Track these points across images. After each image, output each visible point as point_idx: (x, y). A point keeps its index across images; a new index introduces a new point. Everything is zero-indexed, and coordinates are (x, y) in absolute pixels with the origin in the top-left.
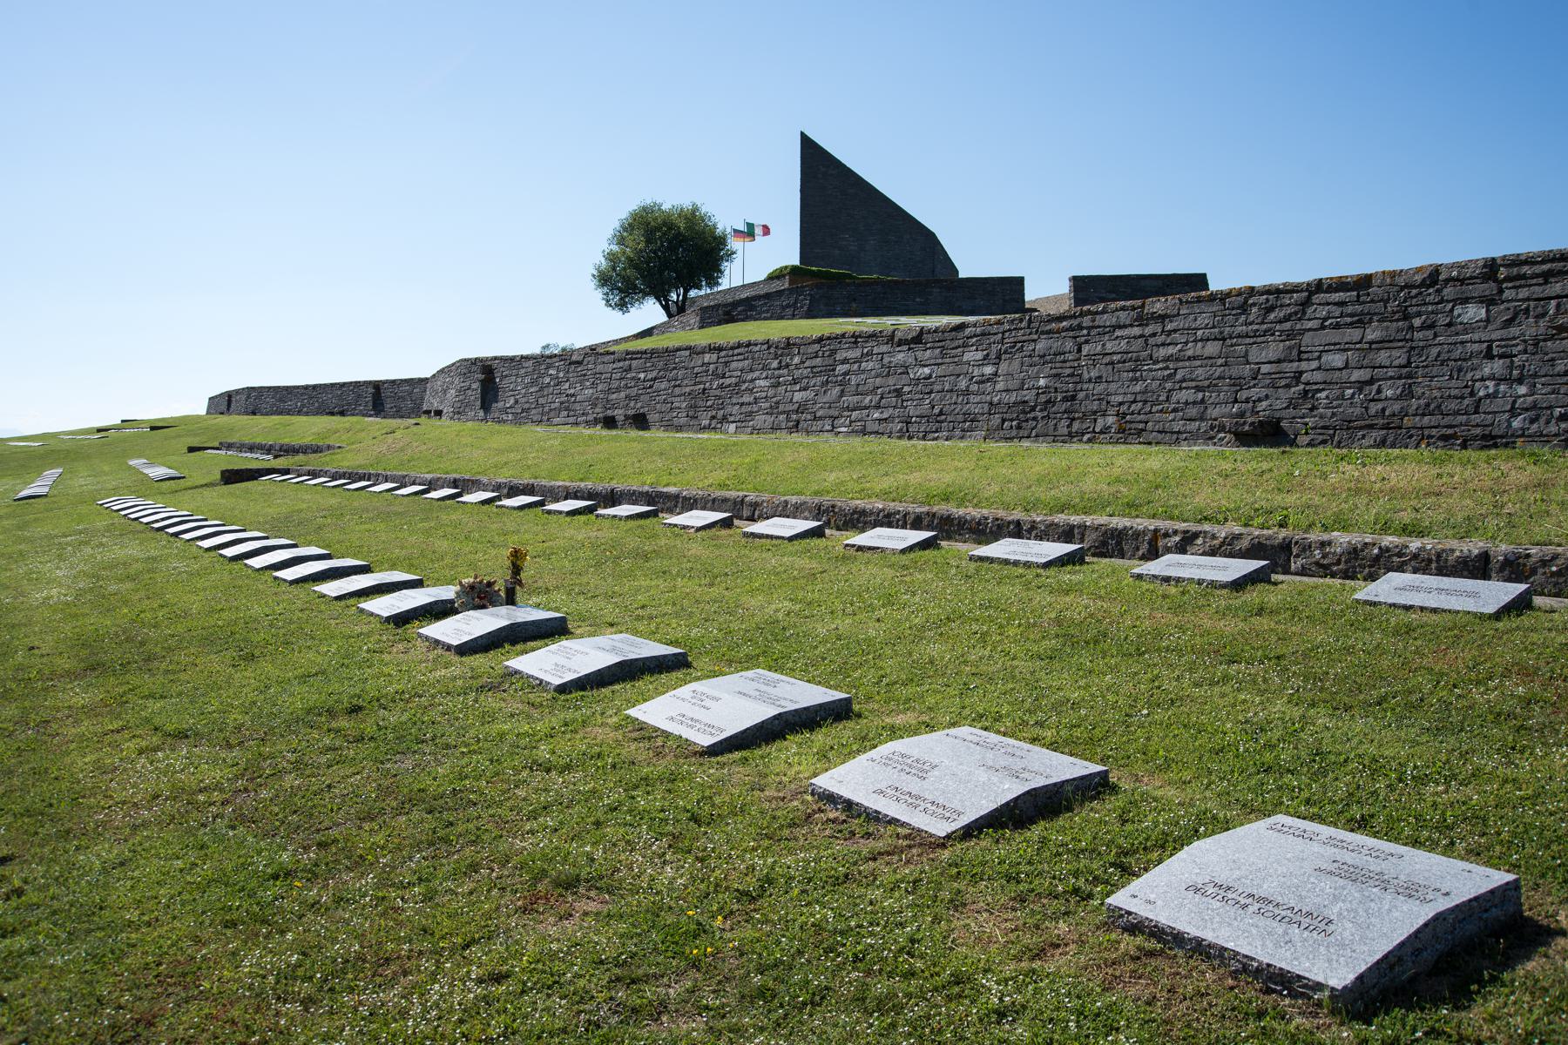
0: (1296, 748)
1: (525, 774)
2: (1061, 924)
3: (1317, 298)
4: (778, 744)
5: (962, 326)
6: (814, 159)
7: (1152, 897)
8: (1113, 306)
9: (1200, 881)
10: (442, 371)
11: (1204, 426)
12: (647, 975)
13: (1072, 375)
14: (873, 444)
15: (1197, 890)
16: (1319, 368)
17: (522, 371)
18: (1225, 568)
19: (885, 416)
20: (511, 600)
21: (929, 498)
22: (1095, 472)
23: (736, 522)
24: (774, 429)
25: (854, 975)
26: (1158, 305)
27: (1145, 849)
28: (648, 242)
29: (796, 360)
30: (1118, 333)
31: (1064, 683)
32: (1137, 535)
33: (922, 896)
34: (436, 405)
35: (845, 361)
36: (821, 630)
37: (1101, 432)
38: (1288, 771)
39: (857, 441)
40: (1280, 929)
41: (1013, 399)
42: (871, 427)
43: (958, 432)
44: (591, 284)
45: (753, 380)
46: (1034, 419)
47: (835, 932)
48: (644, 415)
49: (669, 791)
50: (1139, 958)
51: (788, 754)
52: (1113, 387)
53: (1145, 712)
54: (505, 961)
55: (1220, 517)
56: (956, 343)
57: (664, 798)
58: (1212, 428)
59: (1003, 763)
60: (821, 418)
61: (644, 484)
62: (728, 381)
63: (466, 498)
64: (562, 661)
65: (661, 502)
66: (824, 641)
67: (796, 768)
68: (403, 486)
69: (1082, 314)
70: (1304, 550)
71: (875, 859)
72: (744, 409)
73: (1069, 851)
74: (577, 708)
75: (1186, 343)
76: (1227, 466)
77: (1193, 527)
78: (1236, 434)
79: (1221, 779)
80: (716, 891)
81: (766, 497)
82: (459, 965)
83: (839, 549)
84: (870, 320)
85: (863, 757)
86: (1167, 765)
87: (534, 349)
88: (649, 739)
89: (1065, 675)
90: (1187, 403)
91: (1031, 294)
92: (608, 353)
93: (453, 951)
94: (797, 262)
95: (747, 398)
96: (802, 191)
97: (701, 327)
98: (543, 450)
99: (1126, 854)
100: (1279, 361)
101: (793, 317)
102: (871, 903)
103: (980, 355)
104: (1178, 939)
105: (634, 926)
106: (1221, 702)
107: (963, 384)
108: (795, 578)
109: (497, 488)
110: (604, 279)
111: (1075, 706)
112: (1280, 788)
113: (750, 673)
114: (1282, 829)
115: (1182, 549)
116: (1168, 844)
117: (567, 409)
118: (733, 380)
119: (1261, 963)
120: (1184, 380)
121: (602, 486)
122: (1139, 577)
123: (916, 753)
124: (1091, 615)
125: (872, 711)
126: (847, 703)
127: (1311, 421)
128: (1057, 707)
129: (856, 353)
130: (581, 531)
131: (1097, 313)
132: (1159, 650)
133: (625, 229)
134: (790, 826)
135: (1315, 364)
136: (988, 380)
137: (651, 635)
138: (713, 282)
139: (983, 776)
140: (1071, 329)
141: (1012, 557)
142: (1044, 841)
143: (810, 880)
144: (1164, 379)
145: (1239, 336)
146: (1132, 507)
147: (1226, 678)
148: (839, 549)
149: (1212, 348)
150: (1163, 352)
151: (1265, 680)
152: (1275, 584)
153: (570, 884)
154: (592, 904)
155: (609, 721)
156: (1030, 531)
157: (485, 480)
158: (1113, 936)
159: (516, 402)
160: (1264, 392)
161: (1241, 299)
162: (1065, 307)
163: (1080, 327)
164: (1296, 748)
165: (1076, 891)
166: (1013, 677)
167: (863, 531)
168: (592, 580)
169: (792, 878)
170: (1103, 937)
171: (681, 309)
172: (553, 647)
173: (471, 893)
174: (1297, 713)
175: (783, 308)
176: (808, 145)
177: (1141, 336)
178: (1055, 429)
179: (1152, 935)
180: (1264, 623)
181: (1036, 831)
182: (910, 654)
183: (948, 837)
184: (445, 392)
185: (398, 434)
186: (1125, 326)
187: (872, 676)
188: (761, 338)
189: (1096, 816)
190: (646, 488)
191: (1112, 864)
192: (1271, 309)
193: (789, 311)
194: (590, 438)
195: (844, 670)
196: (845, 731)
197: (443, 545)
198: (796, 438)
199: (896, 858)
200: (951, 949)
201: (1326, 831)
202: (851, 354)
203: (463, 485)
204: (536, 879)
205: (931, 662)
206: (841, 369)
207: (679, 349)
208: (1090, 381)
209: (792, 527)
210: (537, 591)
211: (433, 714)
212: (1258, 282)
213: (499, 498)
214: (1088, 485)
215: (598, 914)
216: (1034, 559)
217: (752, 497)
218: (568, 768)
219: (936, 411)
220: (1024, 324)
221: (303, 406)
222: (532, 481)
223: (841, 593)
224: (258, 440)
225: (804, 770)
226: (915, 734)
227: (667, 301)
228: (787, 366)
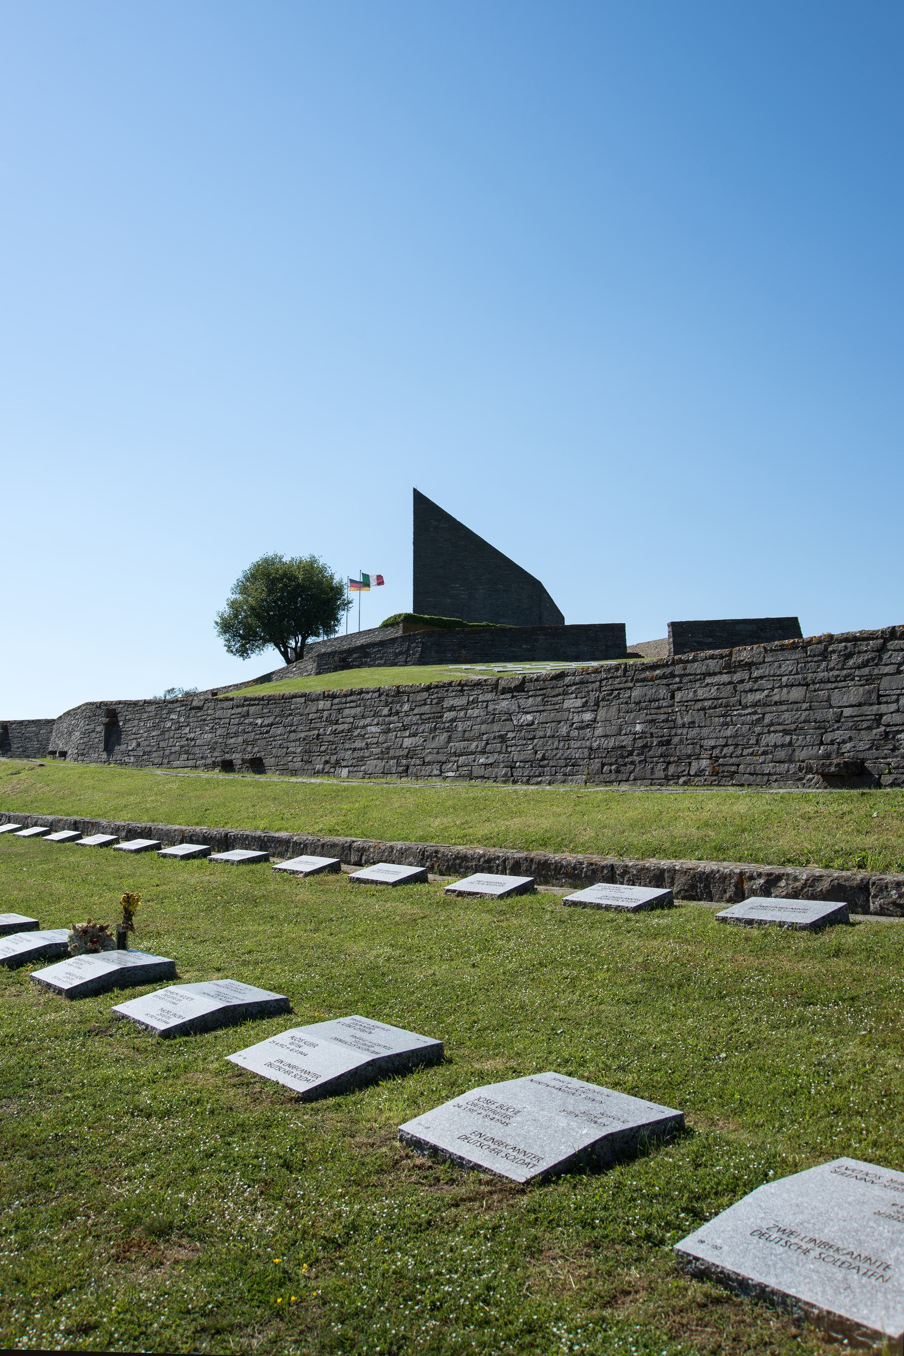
0: (865, 1090)
1: (126, 1119)
2: (633, 1271)
3: (892, 644)
4: (370, 1090)
5: (561, 675)
6: (427, 513)
7: (719, 1242)
8: (702, 655)
9: (764, 1225)
10: (68, 713)
11: (793, 767)
12: (232, 1326)
13: (666, 721)
14: (477, 790)
15: (761, 1235)
16: (898, 711)
17: (145, 715)
18: (805, 910)
19: (490, 761)
20: (122, 944)
21: (529, 843)
22: (687, 815)
23: (344, 867)
24: (385, 773)
25: (431, 1324)
26: (744, 653)
27: (716, 1193)
28: (270, 592)
29: (406, 707)
30: (709, 680)
31: (649, 1028)
32: (724, 878)
33: (501, 1243)
34: (61, 746)
35: (452, 708)
36: (419, 976)
37: (696, 775)
38: (858, 1113)
39: (462, 787)
40: (840, 1275)
41: (611, 745)
42: (477, 771)
43: (560, 777)
44: (215, 631)
45: (364, 727)
46: (632, 763)
47: (415, 1279)
48: (260, 759)
49: (264, 1137)
50: (705, 1305)
51: (378, 1100)
52: (705, 732)
53: (723, 1055)
54: (94, 1311)
55: (803, 859)
56: (557, 691)
57: (258, 1144)
58: (800, 769)
59: (583, 1109)
60: (429, 763)
61: (257, 829)
62: (340, 727)
63: (88, 840)
64: (168, 1006)
65: (274, 847)
66: (420, 988)
67: (387, 1114)
68: (26, 827)
69: (674, 663)
70: (881, 890)
71: (457, 1205)
72: (356, 754)
73: (643, 1196)
74: (180, 1053)
75: (772, 689)
76: (810, 808)
77: (776, 870)
78: (823, 775)
79: (792, 1122)
80: (303, 1239)
81: (372, 842)
82: (48, 1317)
83: (441, 894)
84: (479, 667)
85: (450, 1103)
86: (740, 1111)
87: (158, 692)
88: (248, 1084)
89: (649, 1020)
90: (775, 746)
91: (632, 640)
92: (227, 699)
93: (44, 1301)
94: (410, 610)
95: (359, 744)
97: (318, 673)
98: (161, 793)
99: (698, 1199)
100: (860, 705)
101: (406, 664)
102: (451, 1250)
103: (579, 702)
104: (743, 1285)
105: (222, 1274)
106: (796, 1044)
107: (564, 730)
108: (397, 924)
109: (116, 830)
111: (657, 1050)
112: (848, 1130)
113: (347, 1020)
114: (844, 1173)
115: (766, 892)
116: (737, 1188)
117: (187, 753)
118: (346, 726)
119: (821, 1310)
120: (771, 724)
121: (216, 831)
122: (724, 920)
123: (500, 1099)
124: (677, 959)
125: (463, 1057)
126: (439, 1048)
127: (893, 761)
128: (638, 1052)
129: (463, 701)
130: (195, 876)
131: (688, 661)
132: (739, 993)
133: (247, 580)
134: (377, 1172)
135: (893, 707)
136: (588, 726)
137: (255, 981)
138: (329, 630)
139: (562, 1121)
140: (664, 677)
141: (604, 902)
142: (619, 1186)
143: (394, 1227)
144: (754, 724)
145: (821, 682)
146: (720, 851)
147: (802, 1020)
148: (441, 894)
149: (797, 693)
150: (751, 698)
151: (839, 1022)
152: (853, 925)
153: (162, 1232)
154: (183, 1252)
155: (211, 1066)
156: (622, 875)
157: (104, 822)
158: (682, 1283)
159: (138, 745)
160: (848, 734)
161: (821, 647)
162: (665, 653)
163: (673, 675)
164: (865, 1090)
165: (648, 1237)
166: (599, 1022)
167: (465, 875)
168: (202, 924)
169: (377, 1225)
170: (671, 1283)
171: (299, 655)
172: (160, 992)
173: (66, 1241)
174: (868, 1054)
175: (397, 655)
176: (419, 498)
177: (730, 683)
178: (652, 773)
179: (719, 1281)
180: (840, 964)
181: (612, 1176)
182: (502, 1000)
183: (528, 1182)
184: (70, 734)
185: (23, 775)
186: (715, 674)
187: (464, 1021)
188: (372, 686)
189: (672, 1158)
190: (259, 833)
191: (684, 1210)
192: (850, 656)
193: (402, 658)
194: (208, 781)
195: (438, 1016)
196: (435, 1077)
197: (60, 887)
198: (407, 783)
199: (478, 1204)
200: (526, 1296)
201: (887, 1173)
203: (83, 828)
204: (130, 1227)
205: (522, 1007)
206: (448, 716)
207: (294, 696)
208: (683, 726)
209: (397, 873)
210: (149, 936)
211: (42, 1058)
212: (836, 631)
213: (116, 841)
214: (679, 829)
215: (188, 1262)
216: (625, 904)
217: (359, 842)
218: (168, 1113)
219: (539, 756)
220: (620, 673)
222: (149, 824)
223: (441, 938)
225: (394, 1115)
226: (502, 1079)
227: (286, 647)
228: (397, 713)
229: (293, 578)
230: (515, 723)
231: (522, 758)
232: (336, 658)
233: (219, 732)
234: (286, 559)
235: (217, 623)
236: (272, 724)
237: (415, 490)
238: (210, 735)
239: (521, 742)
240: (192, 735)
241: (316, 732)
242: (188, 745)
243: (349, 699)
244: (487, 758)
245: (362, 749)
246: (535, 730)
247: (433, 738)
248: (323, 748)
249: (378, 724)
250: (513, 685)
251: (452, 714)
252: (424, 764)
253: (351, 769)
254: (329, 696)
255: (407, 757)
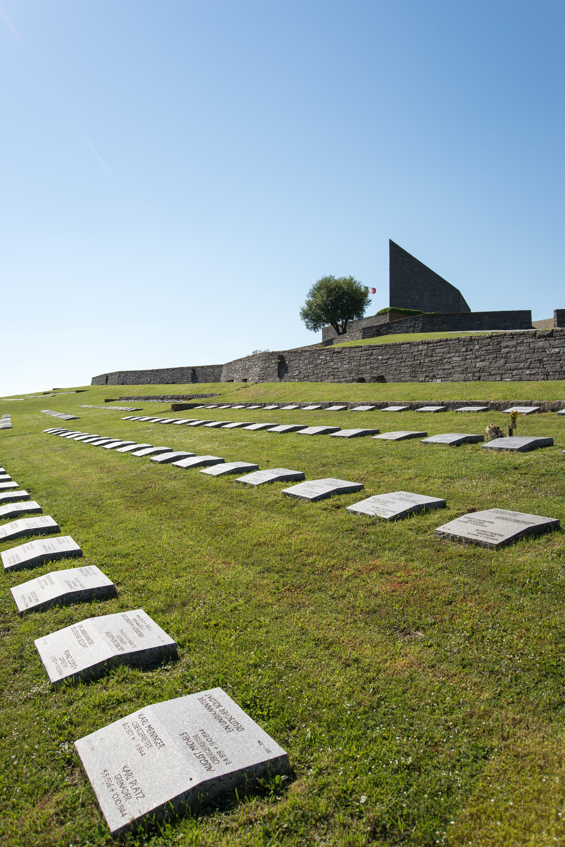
19: (533, 372)
29: (477, 347)
45: (450, 358)
60: (493, 375)
72: (445, 372)
84: (491, 331)
95: (447, 366)
96: (390, 270)
97: (363, 338)
101: (414, 332)
110: (305, 315)
117: (332, 375)
129: (514, 343)
159: (300, 373)
162: (551, 327)
175: (408, 328)
176: (394, 247)
202: (510, 343)
221: (151, 380)
224: (181, 394)
228: (471, 350)
229: (340, 288)
230: (548, 353)
231: (553, 370)
232: (374, 330)
233: (353, 364)
234: (337, 278)
235: (301, 313)
236: (389, 359)
237: (390, 240)
238: (348, 366)
239: (552, 362)
240: (336, 366)
241: (419, 361)
242: (333, 371)
243: (438, 344)
244: (531, 371)
245: (449, 369)
246: (561, 356)
247: (495, 362)
248: (423, 370)
249: (459, 356)
250: (546, 334)
251: (507, 350)
252: (490, 375)
253: (443, 379)
254: (425, 343)
255: (479, 372)
